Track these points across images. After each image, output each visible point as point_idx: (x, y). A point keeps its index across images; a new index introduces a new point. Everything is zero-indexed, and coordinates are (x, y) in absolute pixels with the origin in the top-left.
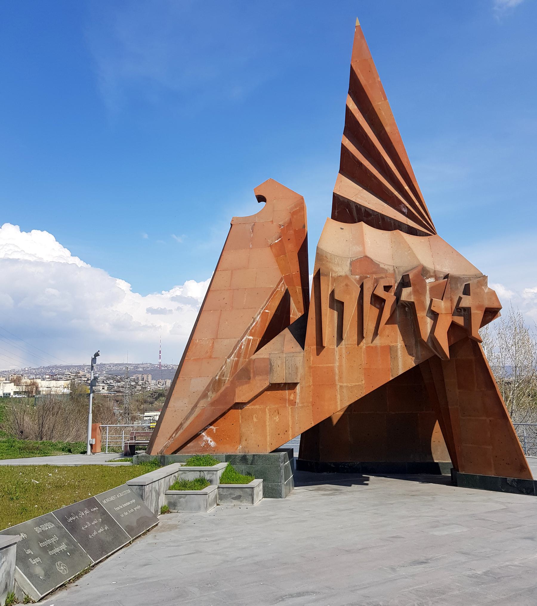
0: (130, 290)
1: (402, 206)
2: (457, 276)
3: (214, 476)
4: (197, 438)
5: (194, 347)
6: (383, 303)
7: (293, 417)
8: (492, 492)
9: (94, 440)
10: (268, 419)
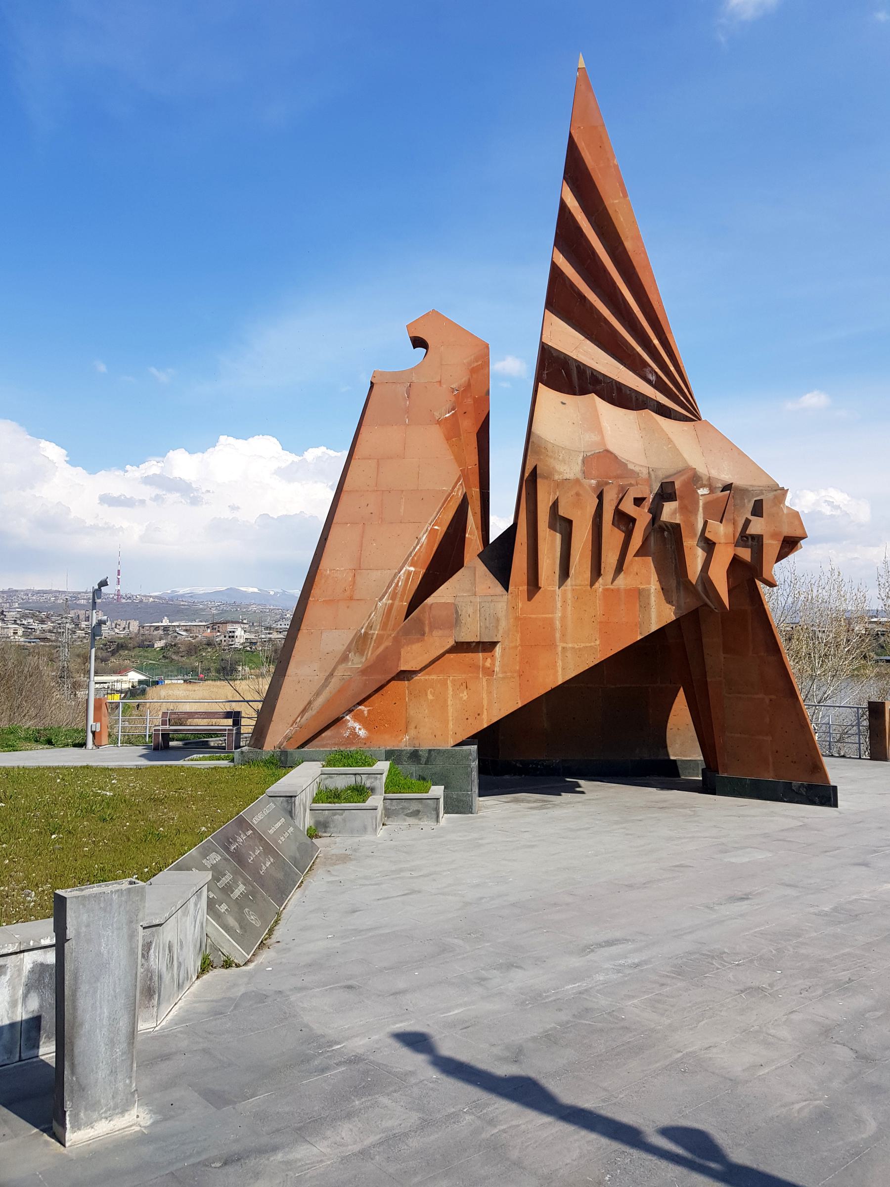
0: (65, 461)
1: (647, 370)
3: (378, 781)
5: (323, 581)
6: (631, 523)
7: (490, 693)
8: (769, 802)
9: (99, 724)
10: (450, 696)
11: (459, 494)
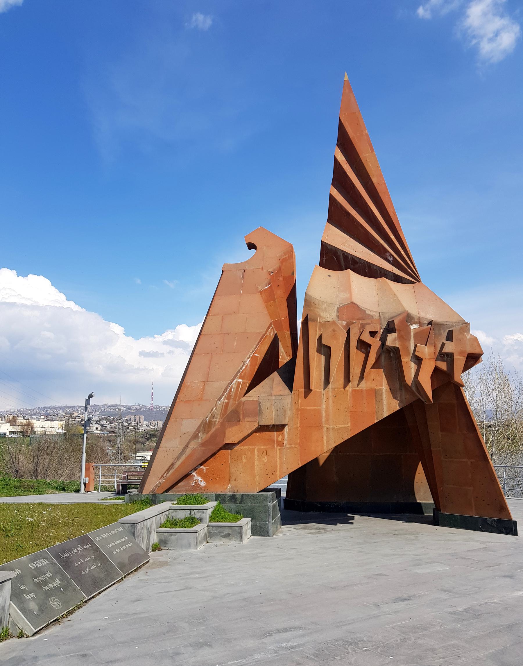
0: (123, 333)
1: (388, 254)
2: (440, 322)
3: (204, 514)
4: (188, 477)
5: (186, 389)
6: (369, 348)
7: (281, 457)
8: (472, 531)
9: (87, 479)
11: (271, 334)
